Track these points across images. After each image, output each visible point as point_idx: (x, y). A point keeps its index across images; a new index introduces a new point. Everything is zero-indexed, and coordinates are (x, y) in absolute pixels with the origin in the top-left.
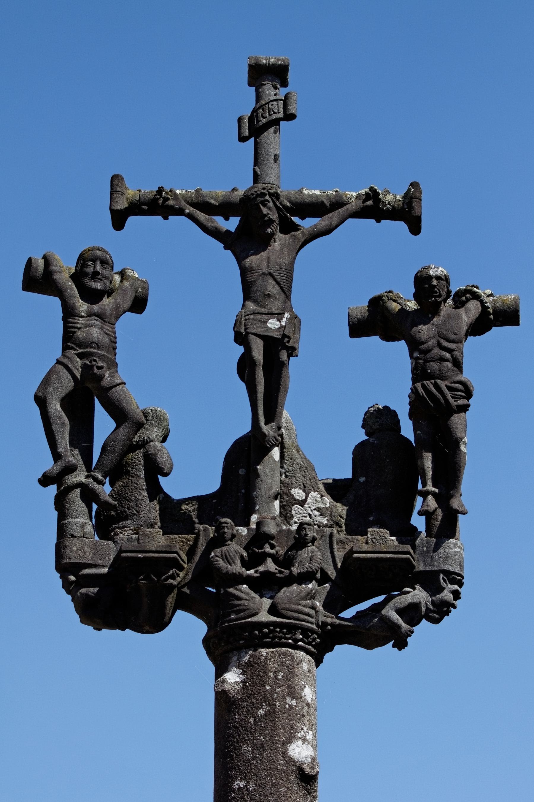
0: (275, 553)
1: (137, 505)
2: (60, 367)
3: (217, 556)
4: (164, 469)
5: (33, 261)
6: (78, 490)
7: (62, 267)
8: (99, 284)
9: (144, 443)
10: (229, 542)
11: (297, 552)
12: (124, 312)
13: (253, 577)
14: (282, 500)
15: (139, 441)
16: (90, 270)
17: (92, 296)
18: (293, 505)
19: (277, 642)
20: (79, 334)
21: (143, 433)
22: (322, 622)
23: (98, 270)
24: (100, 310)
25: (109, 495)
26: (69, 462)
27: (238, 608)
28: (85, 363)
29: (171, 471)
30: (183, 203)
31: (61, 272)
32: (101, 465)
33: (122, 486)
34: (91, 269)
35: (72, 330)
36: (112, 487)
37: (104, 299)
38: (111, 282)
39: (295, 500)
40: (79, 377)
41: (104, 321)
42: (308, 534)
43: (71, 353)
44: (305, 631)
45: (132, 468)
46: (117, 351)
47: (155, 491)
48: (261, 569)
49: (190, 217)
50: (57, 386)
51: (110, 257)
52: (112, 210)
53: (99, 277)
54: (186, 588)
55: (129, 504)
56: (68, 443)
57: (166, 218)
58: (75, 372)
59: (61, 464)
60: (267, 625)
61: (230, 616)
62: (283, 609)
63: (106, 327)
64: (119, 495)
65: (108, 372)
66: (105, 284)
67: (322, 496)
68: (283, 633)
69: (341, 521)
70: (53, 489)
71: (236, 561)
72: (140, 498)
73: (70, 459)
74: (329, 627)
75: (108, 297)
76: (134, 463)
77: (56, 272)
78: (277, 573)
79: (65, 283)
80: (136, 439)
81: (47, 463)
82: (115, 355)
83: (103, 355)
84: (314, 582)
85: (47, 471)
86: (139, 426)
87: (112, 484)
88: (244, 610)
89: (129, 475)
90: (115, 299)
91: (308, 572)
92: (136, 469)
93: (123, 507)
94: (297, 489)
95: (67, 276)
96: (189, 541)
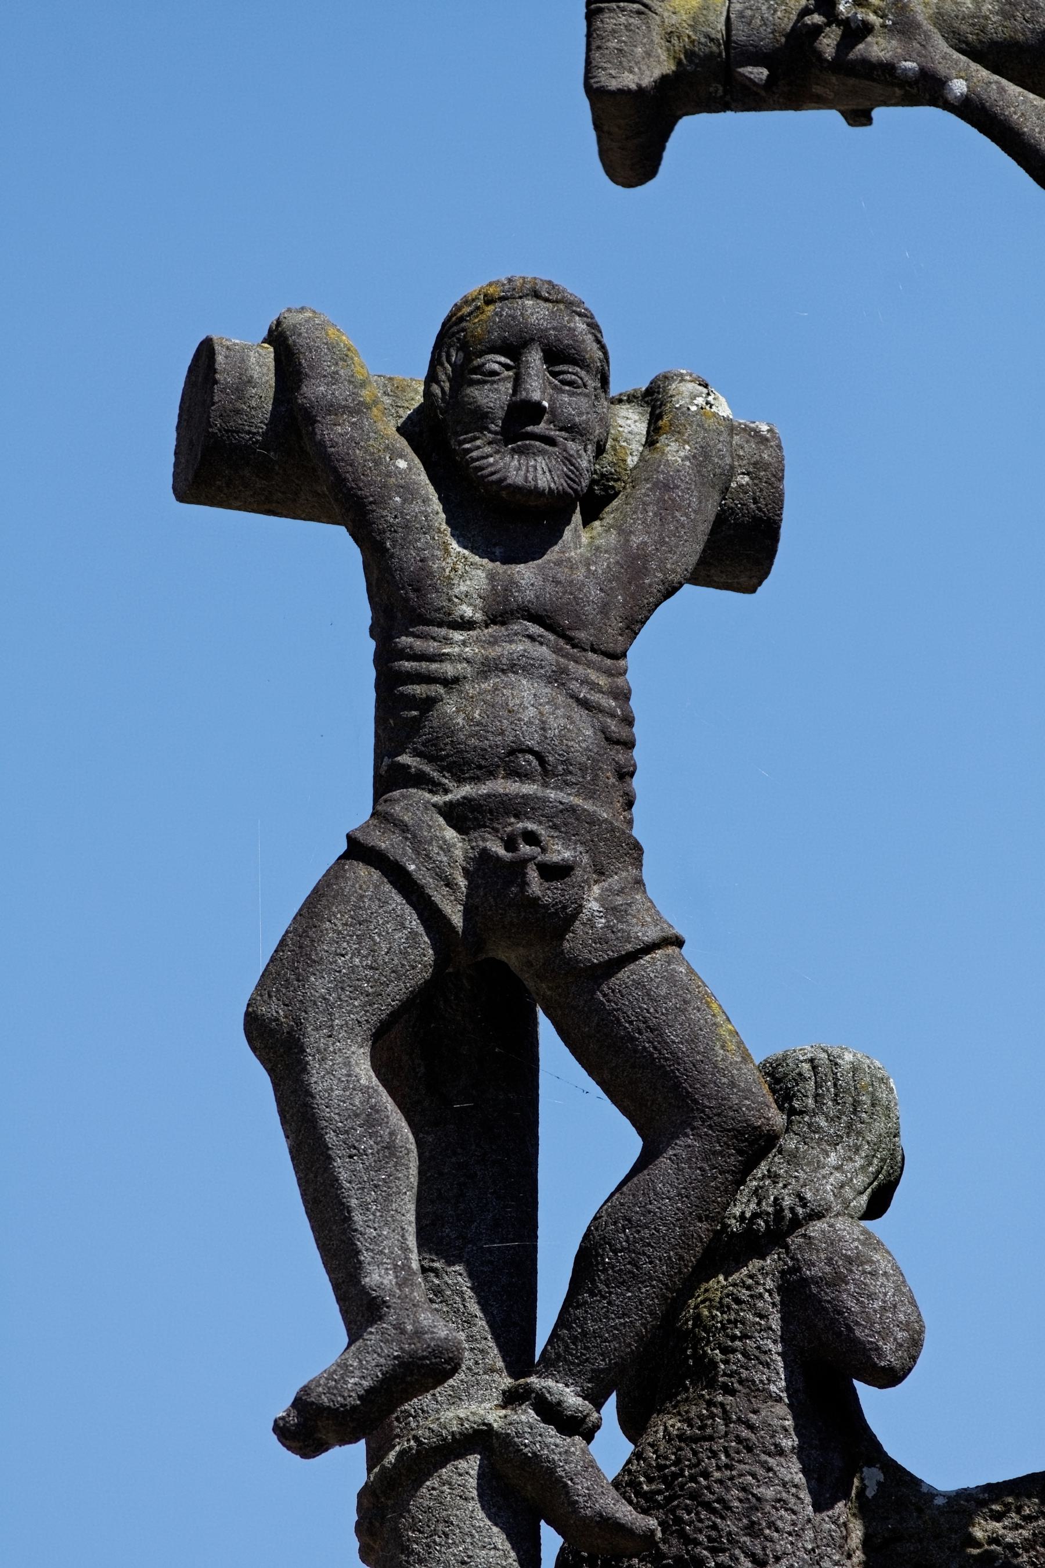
1: (752, 1530)
2: (364, 873)
4: (878, 1349)
5: (220, 359)
6: (471, 1464)
7: (363, 384)
8: (541, 462)
9: (779, 1229)
12: (671, 591)
15: (755, 1215)
16: (493, 397)
17: (511, 524)
20: (451, 709)
21: (774, 1177)
23: (536, 396)
24: (549, 588)
25: (616, 1484)
26: (418, 1333)
28: (484, 852)
29: (914, 1359)
30: (941, 46)
31: (360, 409)
32: (575, 1340)
33: (681, 1437)
34: (500, 365)
35: (418, 690)
36: (632, 1439)
37: (568, 534)
38: (600, 450)
40: (457, 920)
41: (569, 640)
43: (415, 805)
45: (725, 1350)
46: (637, 783)
47: (841, 1451)
49: (976, 113)
50: (353, 969)
51: (594, 327)
52: (595, 93)
53: (541, 428)
55: (714, 1527)
56: (412, 1242)
57: (859, 117)
58: (437, 898)
59: (380, 1351)
63: (580, 670)
64: (669, 1481)
65: (596, 889)
66: (568, 460)
70: (348, 1465)
72: (769, 1493)
73: (426, 1318)
75: (586, 522)
76: (735, 1322)
77: (333, 409)
79: (377, 462)
80: (743, 1206)
81: (313, 1346)
82: (630, 804)
83: (572, 809)
85: (316, 1381)
86: (758, 1144)
87: (633, 1425)
89: (712, 1384)
90: (621, 531)
92: (745, 1354)
93: (688, 1540)
95: (390, 428)
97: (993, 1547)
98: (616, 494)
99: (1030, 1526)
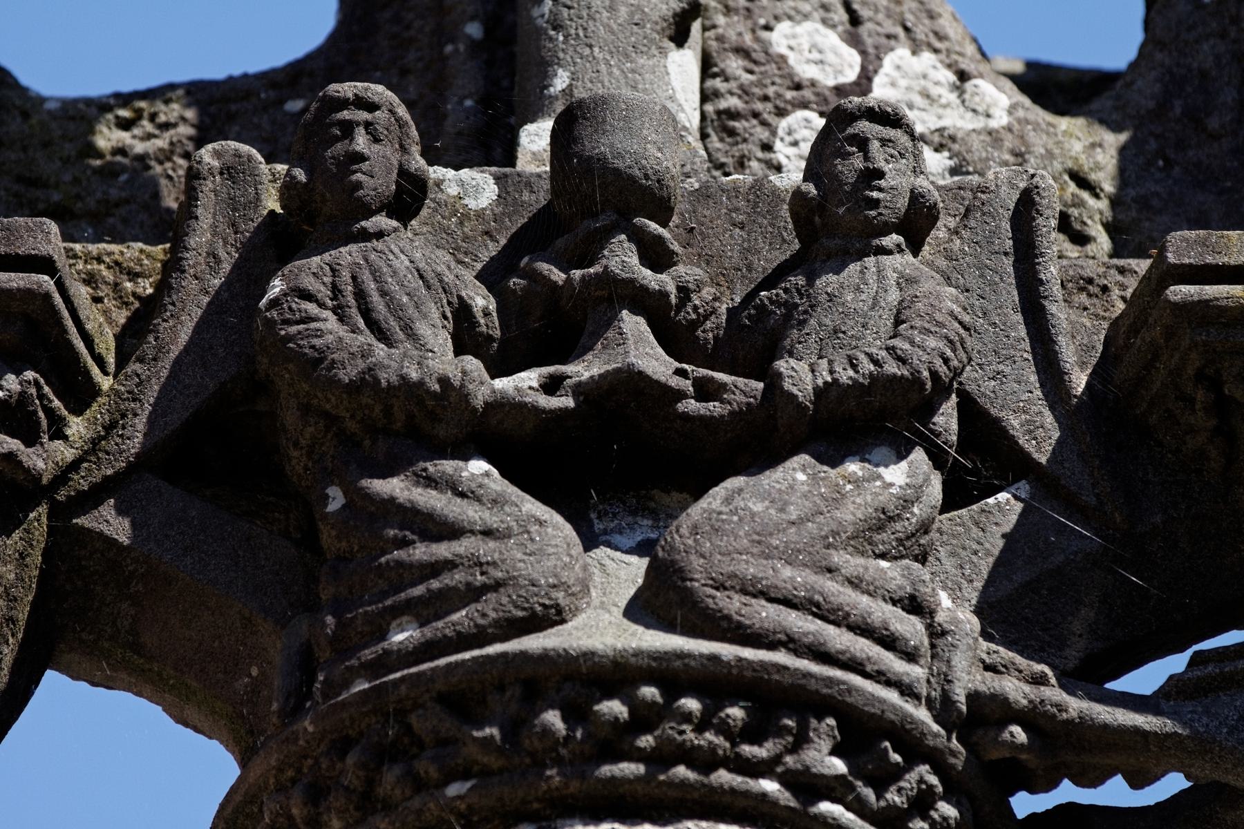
0: (671, 288)
3: (307, 296)
10: (382, 221)
11: (811, 282)
13: (535, 410)
14: (718, 83)
18: (781, 113)
19: (684, 784)
22: (973, 697)
27: (435, 584)
39: (798, 87)
42: (880, 174)
44: (863, 734)
48: (583, 370)
54: (107, 510)
60: (617, 674)
61: (383, 635)
62: (720, 587)
67: (963, 76)
68: (724, 729)
69: (1080, 204)
71: (423, 329)
74: (1018, 733)
78: (681, 395)
84: (919, 455)
88: (474, 594)
91: (880, 382)
94: (808, 26)
96: (133, 276)
97: (119, 158)
98: (664, 107)
99: (167, 135)
